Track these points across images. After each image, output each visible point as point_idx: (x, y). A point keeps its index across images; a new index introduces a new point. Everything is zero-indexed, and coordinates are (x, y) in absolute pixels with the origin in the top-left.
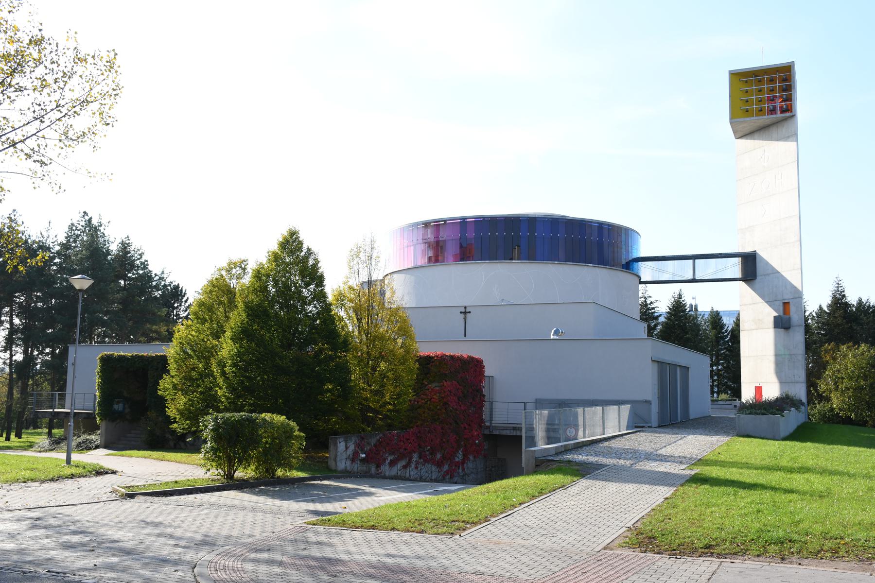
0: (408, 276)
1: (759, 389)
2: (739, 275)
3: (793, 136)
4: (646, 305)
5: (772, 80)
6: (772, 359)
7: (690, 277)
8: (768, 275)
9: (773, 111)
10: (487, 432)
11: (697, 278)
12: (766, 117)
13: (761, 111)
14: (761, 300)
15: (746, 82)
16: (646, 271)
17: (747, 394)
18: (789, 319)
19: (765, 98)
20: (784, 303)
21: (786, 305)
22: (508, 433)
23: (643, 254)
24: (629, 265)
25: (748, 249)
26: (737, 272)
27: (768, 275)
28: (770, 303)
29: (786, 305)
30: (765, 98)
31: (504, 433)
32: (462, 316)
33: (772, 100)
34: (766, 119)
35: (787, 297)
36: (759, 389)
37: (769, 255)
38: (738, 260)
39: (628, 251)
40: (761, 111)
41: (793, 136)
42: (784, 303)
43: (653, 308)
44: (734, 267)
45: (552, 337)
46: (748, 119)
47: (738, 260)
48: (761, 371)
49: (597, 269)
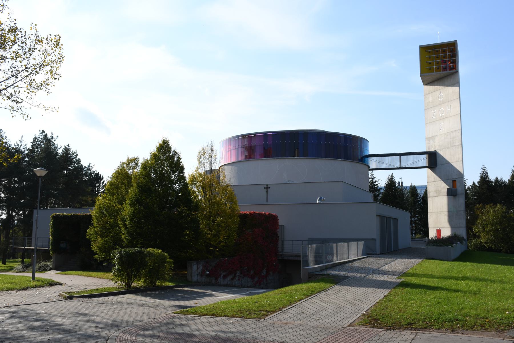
0: (233, 167)
1: (439, 231)
2: (426, 165)
3: (457, 83)
4: (373, 182)
5: (444, 51)
6: (446, 213)
9: (445, 69)
10: (280, 258)
11: (402, 166)
13: (438, 69)
14: (439, 179)
15: (430, 52)
16: (373, 163)
17: (432, 234)
18: (456, 190)
19: (440, 63)
20: (453, 181)
23: (371, 153)
25: (432, 150)
27: (443, 164)
28: (445, 181)
30: (440, 63)
32: (265, 190)
33: (444, 62)
34: (441, 74)
35: (455, 177)
36: (439, 231)
38: (425, 156)
40: (438, 69)
41: (457, 83)
42: (453, 181)
43: (377, 185)
44: (423, 160)
47: (425, 156)
48: (439, 221)
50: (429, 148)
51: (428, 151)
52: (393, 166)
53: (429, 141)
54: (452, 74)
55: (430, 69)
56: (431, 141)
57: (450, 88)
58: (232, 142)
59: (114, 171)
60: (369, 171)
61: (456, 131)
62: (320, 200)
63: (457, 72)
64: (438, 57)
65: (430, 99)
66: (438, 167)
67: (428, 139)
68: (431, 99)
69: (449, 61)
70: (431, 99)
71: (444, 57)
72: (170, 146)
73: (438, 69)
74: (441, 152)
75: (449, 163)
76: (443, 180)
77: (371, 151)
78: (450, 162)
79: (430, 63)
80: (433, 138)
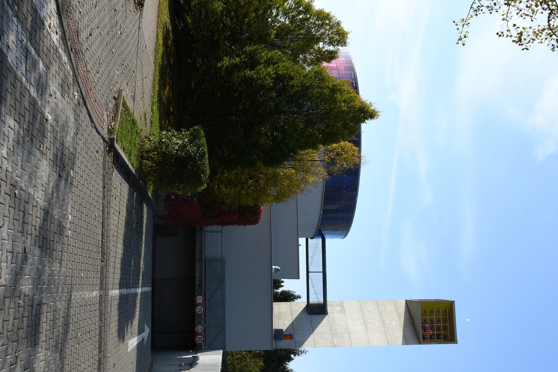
2: (312, 301)
3: (406, 341)
5: (446, 321)
7: (310, 270)
8: (311, 324)
9: (424, 328)
10: (198, 228)
11: (310, 274)
12: (421, 325)
14: (294, 318)
15: (446, 312)
16: (316, 243)
19: (432, 323)
20: (292, 335)
21: (291, 337)
22: (198, 246)
23: (328, 241)
24: (320, 234)
25: (329, 309)
26: (313, 300)
27: (311, 324)
28: (292, 325)
29: (291, 337)
30: (432, 323)
31: (198, 243)
33: (432, 328)
34: (419, 325)
35: (296, 337)
37: (324, 326)
38: (321, 300)
39: (329, 234)
41: (406, 341)
42: (292, 335)
44: (316, 298)
45: (274, 267)
46: (420, 313)
47: (321, 300)
49: (318, 217)
50: (330, 305)
51: (328, 303)
52: (313, 258)
53: (340, 306)
54: (418, 338)
55: (425, 312)
56: (338, 308)
57: (401, 334)
58: (348, 72)
59: (327, 11)
60: (305, 239)
61: (351, 340)
62: (277, 270)
63: (420, 343)
64: (439, 321)
65: (390, 308)
66: (309, 316)
67: (341, 305)
68: (389, 308)
69: (434, 334)
70: (389, 308)
71: (438, 329)
72: (366, 121)
73: (424, 322)
74: (326, 320)
75: (313, 331)
76: (293, 322)
77: (329, 241)
78: (315, 332)
79: (432, 312)
80: (343, 311)
